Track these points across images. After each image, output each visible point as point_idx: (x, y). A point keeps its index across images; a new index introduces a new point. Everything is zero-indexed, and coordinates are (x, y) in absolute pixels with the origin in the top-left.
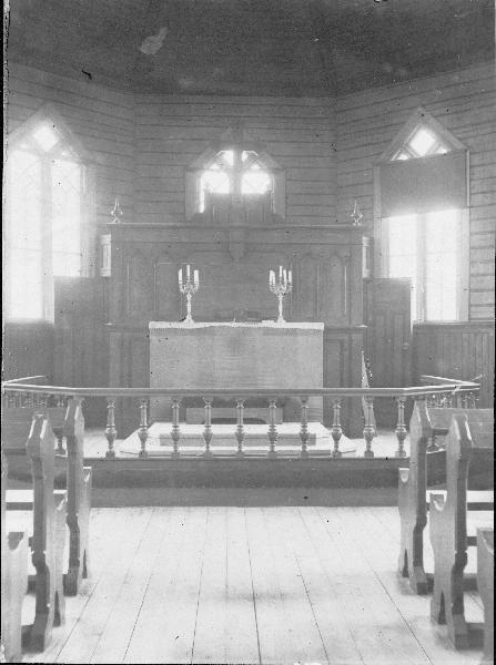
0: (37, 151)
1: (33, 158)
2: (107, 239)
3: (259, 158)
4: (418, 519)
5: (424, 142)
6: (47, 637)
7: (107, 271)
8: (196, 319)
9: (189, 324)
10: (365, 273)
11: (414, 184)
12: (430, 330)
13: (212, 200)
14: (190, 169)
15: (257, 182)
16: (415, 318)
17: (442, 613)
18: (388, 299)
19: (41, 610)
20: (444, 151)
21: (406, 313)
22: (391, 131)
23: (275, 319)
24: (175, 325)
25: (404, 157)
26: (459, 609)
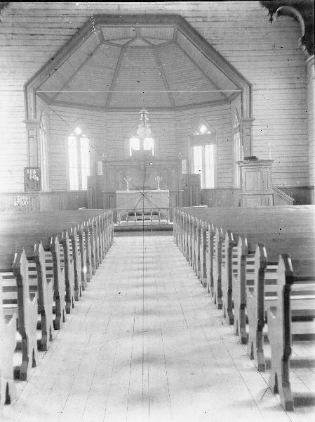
0: (75, 135)
1: (74, 138)
2: (100, 164)
3: (150, 122)
4: (285, 350)
5: (203, 129)
6: (28, 373)
7: (101, 173)
8: (130, 189)
9: (159, 190)
10: (183, 172)
11: (203, 140)
12: (206, 190)
13: (134, 152)
14: (125, 138)
15: (150, 144)
16: (202, 187)
17: (252, 354)
18: (193, 180)
19: (25, 358)
20: (209, 133)
21: (199, 186)
22: (195, 124)
23: (126, 189)
24: (123, 192)
25: (198, 134)
26: (260, 351)
